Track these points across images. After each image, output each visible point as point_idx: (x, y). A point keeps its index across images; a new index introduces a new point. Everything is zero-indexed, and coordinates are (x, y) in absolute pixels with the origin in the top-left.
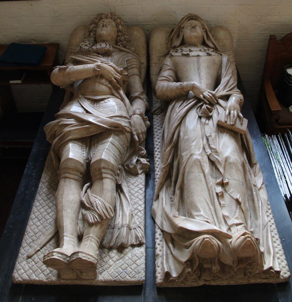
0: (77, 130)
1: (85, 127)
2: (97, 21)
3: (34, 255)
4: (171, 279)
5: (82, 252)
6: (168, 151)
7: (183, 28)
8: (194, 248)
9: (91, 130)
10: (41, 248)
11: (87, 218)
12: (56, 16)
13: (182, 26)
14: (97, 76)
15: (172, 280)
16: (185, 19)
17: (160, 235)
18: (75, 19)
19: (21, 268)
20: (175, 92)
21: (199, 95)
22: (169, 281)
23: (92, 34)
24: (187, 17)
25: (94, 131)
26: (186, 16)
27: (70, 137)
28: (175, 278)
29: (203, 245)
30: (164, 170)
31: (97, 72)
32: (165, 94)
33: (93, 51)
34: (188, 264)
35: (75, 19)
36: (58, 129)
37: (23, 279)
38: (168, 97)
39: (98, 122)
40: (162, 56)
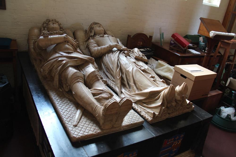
0: (72, 61)
1: (75, 60)
2: (47, 22)
3: (77, 124)
4: (156, 116)
5: (127, 97)
6: (118, 71)
7: (93, 28)
8: (164, 96)
9: (78, 62)
10: (80, 120)
11: (102, 97)
12: (15, 22)
13: (92, 27)
14: (65, 42)
15: (157, 116)
16: (93, 24)
17: (135, 105)
18: (27, 24)
19: (74, 132)
20: (107, 49)
21: (120, 48)
22: (155, 117)
23: (46, 29)
24: (93, 23)
25: (79, 63)
26: (93, 23)
27: (69, 65)
28: (158, 115)
29: (171, 89)
30: (120, 79)
31: (66, 38)
32: (101, 51)
33: (54, 33)
34: (162, 106)
35: (27, 24)
36: (56, 65)
37: (80, 136)
38: (102, 53)
39: (81, 57)
40: (85, 42)
